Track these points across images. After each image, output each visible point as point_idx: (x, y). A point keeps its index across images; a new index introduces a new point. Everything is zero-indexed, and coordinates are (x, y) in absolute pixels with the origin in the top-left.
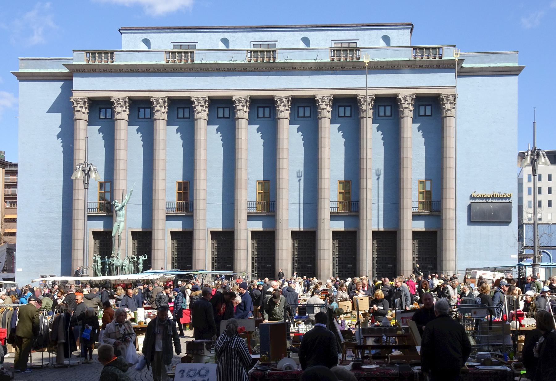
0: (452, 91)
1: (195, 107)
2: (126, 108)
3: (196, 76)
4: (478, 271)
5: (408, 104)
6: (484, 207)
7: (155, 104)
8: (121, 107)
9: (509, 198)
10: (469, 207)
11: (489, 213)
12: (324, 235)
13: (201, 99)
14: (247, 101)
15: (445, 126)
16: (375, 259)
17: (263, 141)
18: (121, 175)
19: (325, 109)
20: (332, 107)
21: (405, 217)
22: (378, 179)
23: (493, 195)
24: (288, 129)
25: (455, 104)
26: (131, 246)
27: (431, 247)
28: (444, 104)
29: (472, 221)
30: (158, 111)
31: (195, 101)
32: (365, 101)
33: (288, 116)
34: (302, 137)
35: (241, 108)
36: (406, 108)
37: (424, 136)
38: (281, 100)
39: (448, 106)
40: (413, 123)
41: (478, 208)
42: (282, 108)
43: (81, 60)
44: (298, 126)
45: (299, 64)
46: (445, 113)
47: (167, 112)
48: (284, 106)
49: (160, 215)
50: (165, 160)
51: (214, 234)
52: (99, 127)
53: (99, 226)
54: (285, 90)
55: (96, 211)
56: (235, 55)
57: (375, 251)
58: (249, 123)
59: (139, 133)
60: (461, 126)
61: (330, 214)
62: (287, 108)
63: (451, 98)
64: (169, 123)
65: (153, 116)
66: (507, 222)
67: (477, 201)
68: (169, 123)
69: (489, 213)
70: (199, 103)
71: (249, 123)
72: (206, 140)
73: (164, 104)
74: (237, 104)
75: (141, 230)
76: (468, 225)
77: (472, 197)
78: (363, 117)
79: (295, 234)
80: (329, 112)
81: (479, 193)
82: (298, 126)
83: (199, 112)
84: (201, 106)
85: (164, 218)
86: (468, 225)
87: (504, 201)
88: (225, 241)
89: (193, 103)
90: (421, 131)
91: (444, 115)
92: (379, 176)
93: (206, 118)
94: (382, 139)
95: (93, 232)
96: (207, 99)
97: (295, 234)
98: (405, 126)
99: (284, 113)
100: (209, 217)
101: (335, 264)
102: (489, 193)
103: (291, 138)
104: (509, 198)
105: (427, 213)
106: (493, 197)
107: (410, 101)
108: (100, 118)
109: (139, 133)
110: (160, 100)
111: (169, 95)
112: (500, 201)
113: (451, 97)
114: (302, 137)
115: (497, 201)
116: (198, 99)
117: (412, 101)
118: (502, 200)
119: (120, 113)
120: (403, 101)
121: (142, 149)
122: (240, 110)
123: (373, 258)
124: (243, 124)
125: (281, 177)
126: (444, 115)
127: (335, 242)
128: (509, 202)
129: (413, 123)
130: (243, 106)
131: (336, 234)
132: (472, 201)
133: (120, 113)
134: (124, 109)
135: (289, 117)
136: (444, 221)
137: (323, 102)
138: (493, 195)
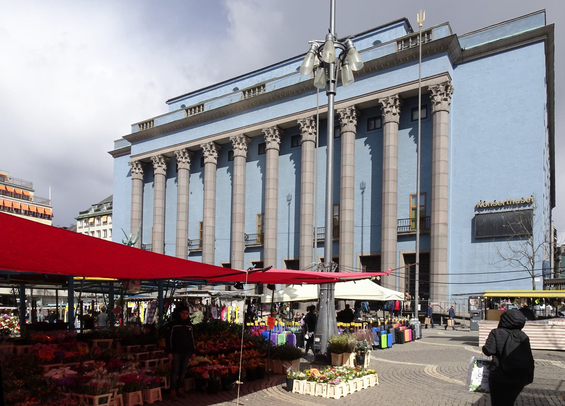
2: (353, 118)
5: (390, 107)
6: (492, 218)
11: (497, 225)
14: (352, 111)
15: (434, 123)
16: (409, 286)
21: (385, 238)
22: (289, 204)
25: (447, 95)
28: (433, 98)
32: (179, 155)
34: (370, 150)
35: (389, 109)
36: (388, 112)
39: (438, 98)
41: (485, 220)
42: (269, 139)
47: (399, 113)
49: (390, 235)
54: (181, 144)
56: (233, 98)
59: (368, 145)
63: (442, 88)
64: (358, 135)
67: (484, 212)
68: (358, 135)
69: (497, 225)
73: (274, 133)
74: (234, 143)
75: (369, 254)
76: (472, 242)
81: (489, 201)
85: (396, 238)
86: (472, 242)
92: (363, 189)
94: (370, 154)
96: (397, 97)
98: (387, 132)
102: (501, 200)
106: (506, 205)
109: (368, 145)
113: (441, 86)
114: (294, 165)
117: (395, 102)
119: (440, 103)
120: (385, 105)
121: (370, 162)
122: (236, 148)
123: (406, 285)
133: (440, 103)
134: (160, 164)
137: (304, 125)
138: (505, 203)
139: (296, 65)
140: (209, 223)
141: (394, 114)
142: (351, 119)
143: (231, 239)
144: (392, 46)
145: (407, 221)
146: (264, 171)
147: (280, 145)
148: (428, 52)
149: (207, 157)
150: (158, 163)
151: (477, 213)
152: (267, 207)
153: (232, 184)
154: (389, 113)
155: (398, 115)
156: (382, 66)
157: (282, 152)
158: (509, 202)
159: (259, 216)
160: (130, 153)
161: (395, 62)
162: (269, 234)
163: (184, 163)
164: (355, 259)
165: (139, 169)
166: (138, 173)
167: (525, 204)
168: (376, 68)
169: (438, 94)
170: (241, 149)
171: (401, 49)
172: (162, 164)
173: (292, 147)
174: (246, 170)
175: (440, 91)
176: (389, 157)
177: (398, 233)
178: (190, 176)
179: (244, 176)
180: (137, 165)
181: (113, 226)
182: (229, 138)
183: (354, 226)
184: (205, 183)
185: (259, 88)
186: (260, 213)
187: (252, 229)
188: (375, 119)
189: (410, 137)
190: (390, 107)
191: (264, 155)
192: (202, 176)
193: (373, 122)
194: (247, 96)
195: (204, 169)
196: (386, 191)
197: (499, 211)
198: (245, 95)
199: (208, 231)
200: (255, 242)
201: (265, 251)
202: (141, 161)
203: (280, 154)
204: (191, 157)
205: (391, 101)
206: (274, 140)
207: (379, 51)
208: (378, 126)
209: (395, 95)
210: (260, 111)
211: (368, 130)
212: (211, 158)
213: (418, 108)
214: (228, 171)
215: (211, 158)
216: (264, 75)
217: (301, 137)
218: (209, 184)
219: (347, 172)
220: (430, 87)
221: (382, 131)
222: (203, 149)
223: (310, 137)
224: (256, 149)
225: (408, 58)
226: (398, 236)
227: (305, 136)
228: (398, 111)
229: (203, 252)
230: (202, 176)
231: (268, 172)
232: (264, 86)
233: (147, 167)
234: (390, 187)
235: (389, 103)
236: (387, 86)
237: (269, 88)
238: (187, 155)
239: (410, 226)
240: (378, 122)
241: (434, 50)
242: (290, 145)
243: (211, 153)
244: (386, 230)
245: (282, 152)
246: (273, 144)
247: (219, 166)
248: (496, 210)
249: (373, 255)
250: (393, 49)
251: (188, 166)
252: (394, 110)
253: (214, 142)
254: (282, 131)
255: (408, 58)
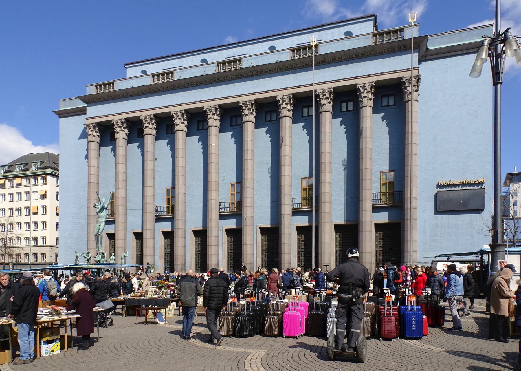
0: (415, 73)
1: (280, 105)
2: (253, 110)
3: (199, 89)
4: (438, 263)
5: (367, 92)
7: (144, 122)
8: (248, 109)
9: (482, 184)
10: (436, 196)
11: (454, 202)
12: (284, 230)
13: (179, 113)
16: (338, 252)
17: (236, 145)
18: (120, 185)
19: (285, 108)
20: (374, 94)
21: (364, 209)
23: (463, 182)
24: (331, 123)
26: (297, 241)
27: (393, 238)
28: (406, 88)
29: (438, 211)
30: (146, 127)
31: (174, 115)
32: (146, 121)
33: (331, 109)
34: (345, 130)
35: (285, 106)
36: (365, 97)
37: (387, 125)
38: (245, 104)
40: (373, 114)
41: (445, 196)
43: (91, 91)
44: (267, 128)
45: (260, 68)
46: (407, 97)
48: (249, 109)
49: (367, 205)
50: (330, 153)
51: (263, 231)
52: (167, 140)
53: (231, 224)
55: (299, 206)
56: (207, 69)
57: (338, 244)
58: (294, 122)
60: (422, 111)
61: (372, 206)
62: (329, 101)
63: (414, 81)
64: (375, 111)
65: (279, 115)
66: (480, 210)
68: (375, 111)
69: (454, 202)
70: (177, 116)
71: (294, 122)
72: (253, 141)
74: (208, 113)
76: (435, 215)
77: (439, 186)
78: (322, 112)
79: (338, 228)
80: (370, 99)
81: (444, 181)
82: (267, 128)
83: (178, 125)
84: (179, 119)
86: (435, 215)
87: (476, 187)
88: (272, 235)
89: (241, 107)
90: (385, 121)
91: (406, 99)
93: (254, 120)
94: (345, 133)
95: (260, 228)
97: (338, 228)
98: (364, 115)
99: (367, 101)
100: (190, 219)
101: (264, 258)
103: (333, 131)
104: (482, 184)
105: (388, 204)
106: (463, 184)
107: (369, 90)
108: (302, 117)
110: (179, 113)
111: (220, 103)
112: (472, 188)
114: (345, 130)
115: (467, 188)
116: (177, 113)
117: (371, 89)
118: (455, 188)
120: (362, 90)
122: (211, 118)
123: (336, 251)
124: (367, 112)
125: (245, 177)
126: (406, 99)
127: (338, 236)
128: (481, 189)
129: (373, 114)
130: (287, 104)
131: (379, 227)
132: (439, 189)
134: (122, 128)
135: (331, 110)
136: (405, 211)
137: (283, 101)
138: (463, 182)
139: (268, 44)
140: (121, 193)
141: (289, 111)
142: (251, 111)
143: (142, 210)
144: (368, 38)
145: (379, 194)
146: (173, 149)
147: (128, 135)
148: (402, 48)
149: (118, 132)
150: (121, 127)
151: (439, 189)
152: (176, 182)
153: (143, 159)
154: (366, 98)
155: (291, 111)
156: (360, 55)
157: (189, 134)
158: (466, 182)
159: (168, 190)
160: (85, 114)
161: (372, 53)
162: (247, 202)
163: (94, 136)
164: (255, 230)
165: (96, 132)
166: (95, 136)
167: (479, 184)
168: (354, 56)
169: (324, 98)
170: (216, 120)
171: (294, 57)
172: (124, 128)
173: (167, 134)
174: (157, 148)
175: (325, 95)
176: (366, 137)
177: (373, 205)
178: (100, 149)
179: (126, 156)
180: (94, 127)
181: (60, 190)
182: (203, 107)
183: (185, 206)
184: (117, 157)
185: (234, 61)
186: (234, 181)
187: (162, 202)
188: (236, 117)
189: (383, 121)
190: (367, 92)
191: (241, 126)
192: (114, 150)
193: (234, 119)
194: (155, 80)
195: (115, 143)
196: (364, 167)
197: (457, 189)
198: (154, 79)
199: (120, 203)
200: (164, 213)
201: (175, 222)
202: (99, 124)
203: (221, 131)
204: (129, 128)
205: (368, 88)
206: (183, 123)
207: (356, 41)
208: (239, 123)
209: (372, 82)
210: (236, 84)
211: (231, 126)
212: (122, 134)
213: (392, 95)
214: (112, 150)
215: (122, 134)
216: (234, 49)
217: (143, 131)
218: (121, 159)
219: (326, 148)
220: (404, 79)
221: (242, 127)
222: (114, 125)
223: (150, 132)
224: (136, 134)
225: (384, 51)
226: (373, 208)
227: (146, 131)
228: (292, 108)
229: (116, 221)
230: (114, 150)
231: (176, 151)
232: (240, 60)
233: (106, 132)
234: (286, 171)
235: (366, 89)
236: (364, 73)
237: (245, 64)
238: (97, 129)
239: (380, 199)
240: (239, 119)
241: (402, 47)
242: (109, 138)
243: (182, 121)
244: (364, 202)
245: (189, 134)
246: (214, 121)
247: (129, 142)
248: (473, 186)
249: (349, 223)
250: (286, 57)
251: (154, 132)
252: (289, 107)
253: (186, 110)
254: (189, 115)
255: (384, 51)
